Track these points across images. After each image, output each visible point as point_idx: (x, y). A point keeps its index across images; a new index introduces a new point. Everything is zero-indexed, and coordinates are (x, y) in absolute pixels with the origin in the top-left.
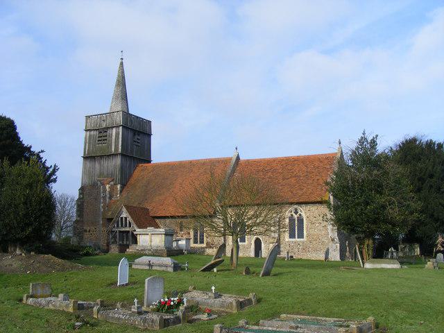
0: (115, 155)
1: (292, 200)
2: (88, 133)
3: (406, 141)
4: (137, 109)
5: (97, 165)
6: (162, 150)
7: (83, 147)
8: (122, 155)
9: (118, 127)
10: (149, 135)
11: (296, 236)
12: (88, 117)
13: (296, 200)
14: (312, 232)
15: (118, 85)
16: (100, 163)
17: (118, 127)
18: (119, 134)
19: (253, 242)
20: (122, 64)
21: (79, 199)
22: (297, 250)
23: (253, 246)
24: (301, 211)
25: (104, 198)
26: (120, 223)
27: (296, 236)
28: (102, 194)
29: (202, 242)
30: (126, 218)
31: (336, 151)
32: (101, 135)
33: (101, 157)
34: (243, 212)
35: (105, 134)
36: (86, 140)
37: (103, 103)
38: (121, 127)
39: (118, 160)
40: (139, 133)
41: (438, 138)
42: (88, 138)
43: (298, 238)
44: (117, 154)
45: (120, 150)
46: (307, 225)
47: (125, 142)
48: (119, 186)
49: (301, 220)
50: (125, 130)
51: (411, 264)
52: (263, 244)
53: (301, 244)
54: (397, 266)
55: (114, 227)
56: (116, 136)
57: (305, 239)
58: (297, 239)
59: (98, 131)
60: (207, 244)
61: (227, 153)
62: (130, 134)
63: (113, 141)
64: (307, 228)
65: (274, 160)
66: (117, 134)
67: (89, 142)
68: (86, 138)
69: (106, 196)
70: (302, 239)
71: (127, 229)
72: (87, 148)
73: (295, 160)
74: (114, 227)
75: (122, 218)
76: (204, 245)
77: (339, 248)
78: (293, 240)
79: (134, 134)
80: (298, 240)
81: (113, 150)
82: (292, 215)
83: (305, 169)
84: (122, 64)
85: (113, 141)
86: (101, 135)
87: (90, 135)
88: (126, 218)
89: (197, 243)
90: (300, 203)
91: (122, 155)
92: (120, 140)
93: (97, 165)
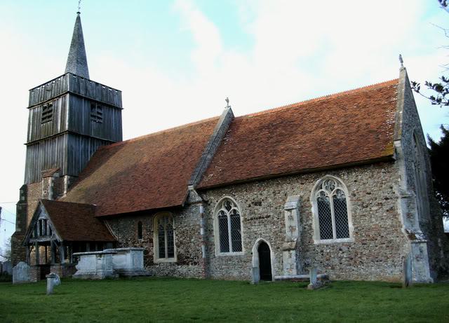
0: (60, 135)
1: (319, 165)
4: (99, 72)
5: (41, 152)
6: (136, 124)
7: (27, 134)
8: (72, 133)
10: (119, 109)
11: (166, 255)
12: (32, 90)
13: (327, 163)
14: (364, 223)
15: (73, 45)
19: (254, 250)
20: (78, 19)
21: (20, 202)
22: (336, 261)
23: (255, 258)
24: (236, 206)
26: (38, 230)
27: (166, 255)
28: (43, 192)
29: (171, 255)
30: (45, 220)
31: (397, 77)
36: (29, 122)
37: (55, 66)
38: (68, 95)
39: (65, 141)
40: (101, 105)
43: (234, 251)
45: (67, 127)
46: (354, 210)
48: (66, 179)
49: (340, 205)
50: (74, 99)
52: (272, 254)
53: (345, 249)
54: (201, 212)
55: (31, 237)
56: (63, 107)
57: (351, 239)
58: (335, 240)
59: (42, 102)
60: (179, 257)
61: (213, 110)
62: (85, 107)
63: (60, 115)
64: (354, 217)
66: (64, 105)
67: (34, 123)
70: (346, 240)
72: (31, 132)
76: (174, 260)
77: (426, 253)
78: (329, 241)
79: (93, 107)
80: (339, 240)
81: (59, 128)
82: (322, 193)
83: (342, 113)
84: (78, 19)
88: (45, 220)
89: (164, 257)
90: (337, 169)
91: (72, 133)
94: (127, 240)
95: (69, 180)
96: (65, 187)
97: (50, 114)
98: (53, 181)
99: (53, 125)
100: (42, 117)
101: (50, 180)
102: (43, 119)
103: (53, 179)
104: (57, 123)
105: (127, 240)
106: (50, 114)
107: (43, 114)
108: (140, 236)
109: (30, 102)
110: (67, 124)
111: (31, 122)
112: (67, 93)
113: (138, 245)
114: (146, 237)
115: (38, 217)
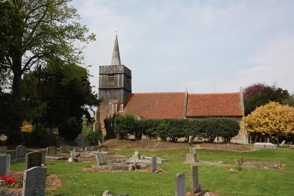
2: (102, 76)
10: (131, 78)
17: (121, 74)
18: (121, 80)
20: (117, 38)
38: (123, 75)
44: (121, 88)
47: (119, 79)
48: (122, 105)
51: (193, 176)
56: (120, 80)
63: (118, 81)
65: (207, 95)
66: (121, 78)
68: (100, 78)
69: (115, 110)
72: (101, 84)
73: (218, 95)
81: (118, 85)
84: (117, 38)
85: (118, 81)
87: (103, 77)
91: (124, 88)
92: (123, 80)
93: (108, 93)
95: (124, 105)
96: (122, 108)
97: (113, 79)
98: (117, 105)
99: (115, 84)
101: (116, 105)
106: (113, 79)
110: (123, 85)
111: (101, 79)
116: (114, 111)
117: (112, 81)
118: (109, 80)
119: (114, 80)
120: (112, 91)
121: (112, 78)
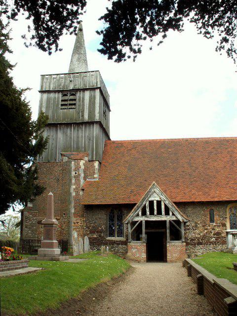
2: (45, 96)
3: (39, 48)
9: (93, 89)
16: (65, 133)
25: (77, 177)
28: (73, 173)
30: (159, 203)
32: (66, 98)
33: (68, 125)
34: (65, 283)
35: (72, 97)
41: (228, 132)
42: (44, 105)
48: (96, 164)
55: (138, 215)
69: (79, 175)
71: (163, 218)
74: (138, 215)
75: (151, 203)
86: (66, 98)
87: (48, 100)
88: (159, 203)
94: (196, 223)
97: (73, 102)
100: (60, 103)
102: (62, 105)
103: (84, 162)
104: (83, 112)
105: (196, 223)
106: (73, 102)
107: (62, 101)
108: (212, 220)
109: (42, 87)
112: (97, 88)
113: (209, 228)
114: (219, 222)
115: (150, 197)
116: (75, 177)
117: (70, 107)
118: (62, 105)
119: (75, 104)
120: (71, 131)
121: (71, 100)
